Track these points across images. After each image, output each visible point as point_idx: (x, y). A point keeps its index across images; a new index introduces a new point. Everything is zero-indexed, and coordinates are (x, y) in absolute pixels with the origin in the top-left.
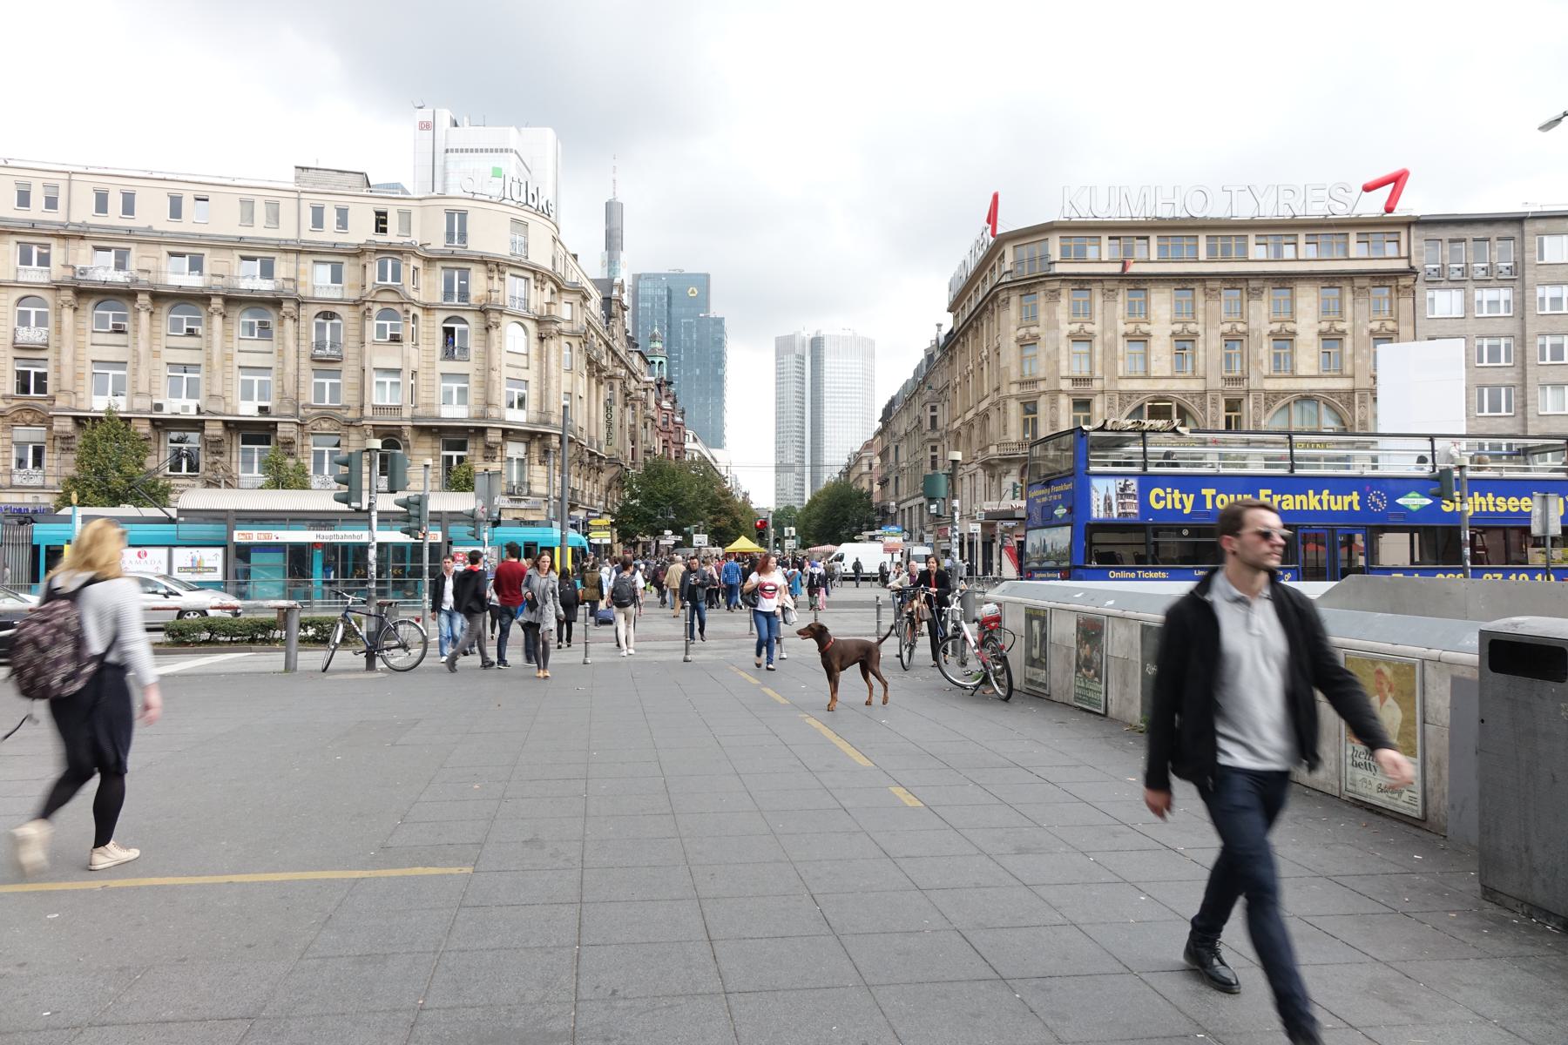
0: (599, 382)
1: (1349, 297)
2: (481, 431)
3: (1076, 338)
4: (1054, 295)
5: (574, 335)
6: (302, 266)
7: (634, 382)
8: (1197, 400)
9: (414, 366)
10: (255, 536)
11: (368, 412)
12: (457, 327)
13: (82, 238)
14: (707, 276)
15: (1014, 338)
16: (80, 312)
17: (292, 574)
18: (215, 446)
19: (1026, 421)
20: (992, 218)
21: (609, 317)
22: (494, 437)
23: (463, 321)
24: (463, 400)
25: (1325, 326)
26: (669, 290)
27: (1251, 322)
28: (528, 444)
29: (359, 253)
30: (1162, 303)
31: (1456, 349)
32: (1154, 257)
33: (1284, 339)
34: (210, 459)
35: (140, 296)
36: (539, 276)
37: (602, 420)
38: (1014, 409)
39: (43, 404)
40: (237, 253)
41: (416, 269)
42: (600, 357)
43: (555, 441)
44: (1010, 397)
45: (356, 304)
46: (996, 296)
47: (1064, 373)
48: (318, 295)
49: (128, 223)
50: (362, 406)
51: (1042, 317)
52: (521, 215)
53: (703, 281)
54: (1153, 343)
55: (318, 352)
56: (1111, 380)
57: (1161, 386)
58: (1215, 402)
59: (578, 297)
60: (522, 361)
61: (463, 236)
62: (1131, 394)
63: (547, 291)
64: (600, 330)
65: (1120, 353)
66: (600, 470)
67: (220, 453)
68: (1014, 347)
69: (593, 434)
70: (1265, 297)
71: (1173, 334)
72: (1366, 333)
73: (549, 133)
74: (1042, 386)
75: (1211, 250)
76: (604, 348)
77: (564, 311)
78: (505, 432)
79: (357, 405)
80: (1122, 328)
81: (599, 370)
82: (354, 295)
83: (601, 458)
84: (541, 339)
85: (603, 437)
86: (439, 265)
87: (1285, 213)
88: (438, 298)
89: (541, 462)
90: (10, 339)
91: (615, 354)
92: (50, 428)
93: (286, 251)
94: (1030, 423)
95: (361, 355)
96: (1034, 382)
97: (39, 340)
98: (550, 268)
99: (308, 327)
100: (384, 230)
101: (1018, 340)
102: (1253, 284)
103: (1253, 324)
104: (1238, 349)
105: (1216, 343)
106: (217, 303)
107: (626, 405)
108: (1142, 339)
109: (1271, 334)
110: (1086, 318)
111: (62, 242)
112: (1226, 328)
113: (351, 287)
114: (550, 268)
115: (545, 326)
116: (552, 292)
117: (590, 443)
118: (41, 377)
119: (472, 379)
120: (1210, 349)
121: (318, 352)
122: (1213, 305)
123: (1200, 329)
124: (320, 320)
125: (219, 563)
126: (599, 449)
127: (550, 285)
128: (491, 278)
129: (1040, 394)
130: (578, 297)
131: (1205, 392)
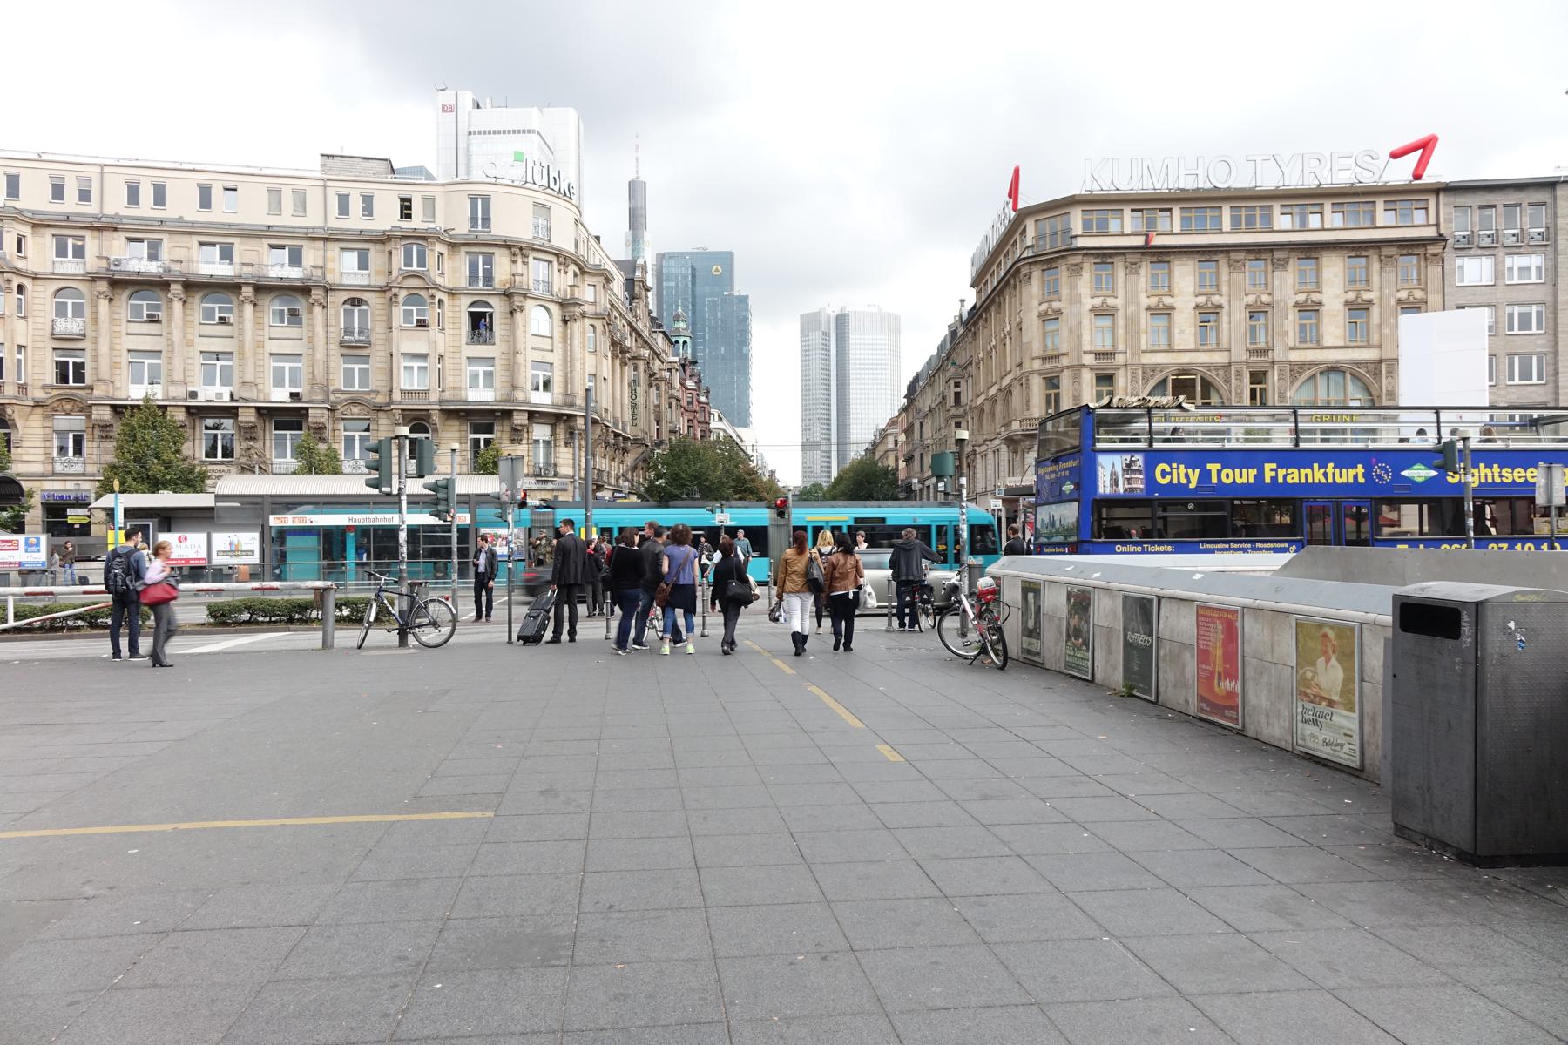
0: (624, 364)
1: (1376, 266)
2: (508, 414)
3: (1098, 312)
4: (1076, 269)
5: (597, 317)
6: (329, 253)
7: (658, 362)
9: (441, 350)
10: (291, 520)
13: (116, 229)
14: (731, 254)
15: (1035, 313)
18: (249, 432)
19: (1049, 396)
20: (1014, 193)
21: (633, 297)
22: (521, 419)
23: (360, 302)
25: (1351, 296)
26: (693, 269)
28: (553, 426)
29: (384, 239)
32: (1177, 229)
33: (1310, 310)
34: (244, 445)
36: (562, 258)
38: (1037, 384)
40: (266, 242)
41: (441, 254)
42: (624, 338)
44: (1033, 372)
45: (383, 290)
46: (1018, 271)
47: (1087, 348)
49: (159, 214)
50: (391, 391)
52: (543, 198)
53: (727, 259)
55: (347, 338)
56: (1134, 354)
57: (1185, 359)
58: (1239, 374)
59: (601, 279)
60: (546, 344)
61: (486, 221)
62: (1155, 368)
63: (570, 274)
64: (624, 311)
65: (1143, 327)
66: (625, 451)
67: (253, 439)
68: (1036, 322)
70: (1290, 267)
71: (1197, 306)
72: (1393, 302)
73: (571, 114)
74: (1065, 361)
75: (1236, 221)
76: (627, 329)
77: (587, 293)
78: (531, 414)
79: (386, 389)
80: (1145, 301)
81: (623, 352)
82: (380, 281)
84: (565, 322)
85: (628, 418)
86: (463, 250)
87: (1311, 183)
88: (463, 283)
89: (566, 444)
91: (639, 335)
93: (314, 239)
96: (1056, 357)
97: (76, 331)
98: (573, 250)
99: (337, 314)
100: (409, 216)
101: (1040, 315)
102: (1278, 254)
104: (1262, 321)
105: (1240, 315)
106: (247, 291)
107: (651, 386)
108: (1166, 312)
111: (96, 233)
112: (1251, 299)
113: (378, 273)
114: (573, 250)
115: (568, 309)
116: (576, 275)
117: (615, 424)
118: (79, 367)
119: (497, 362)
120: (1234, 321)
121: (347, 338)
123: (1223, 301)
125: (256, 547)
126: (624, 429)
127: (572, 268)
128: (514, 262)
129: (1063, 368)
130: (601, 279)
131: (1230, 364)
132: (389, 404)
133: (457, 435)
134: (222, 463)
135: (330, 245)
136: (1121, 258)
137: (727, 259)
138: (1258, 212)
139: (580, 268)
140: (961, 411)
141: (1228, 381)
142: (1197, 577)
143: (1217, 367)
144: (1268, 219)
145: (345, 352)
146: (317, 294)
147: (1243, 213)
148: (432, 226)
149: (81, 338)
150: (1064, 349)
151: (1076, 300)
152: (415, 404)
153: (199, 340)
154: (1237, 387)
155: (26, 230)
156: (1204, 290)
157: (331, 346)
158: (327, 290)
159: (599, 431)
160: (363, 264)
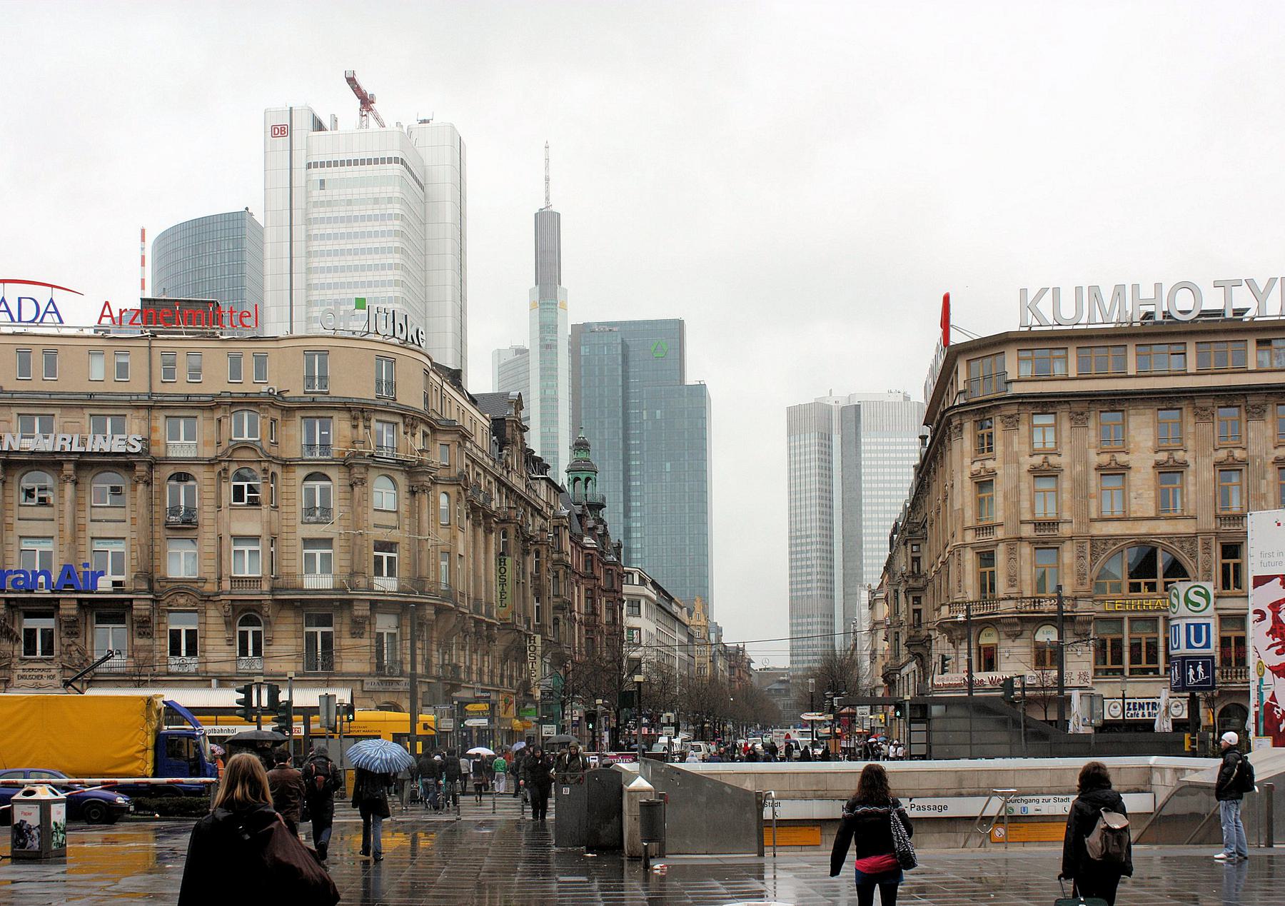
0: (488, 531)
2: (349, 603)
4: (1012, 422)
7: (539, 521)
8: (1187, 545)
11: (226, 585)
14: (680, 324)
15: (967, 474)
16: (80, 486)
18: (72, 627)
19: (1225, 568)
21: (502, 443)
22: (361, 610)
24: (326, 569)
26: (625, 347)
27: (1252, 447)
28: (400, 616)
30: (1142, 431)
34: (66, 641)
36: (411, 419)
38: (969, 558)
43: (430, 612)
44: (964, 546)
45: (211, 463)
46: (949, 422)
47: (1026, 516)
50: (220, 579)
51: (999, 447)
53: (673, 332)
55: (173, 519)
57: (1143, 528)
58: (1207, 547)
59: (455, 437)
60: (391, 520)
62: (1107, 539)
63: (419, 435)
65: (1093, 490)
66: (491, 639)
67: (76, 634)
68: (969, 486)
70: (1269, 417)
71: (1157, 465)
74: (1000, 533)
77: (437, 456)
78: (373, 604)
79: (214, 577)
80: (1095, 460)
81: (486, 516)
82: (209, 453)
83: (490, 626)
84: (413, 493)
86: (299, 414)
91: (510, 490)
94: (986, 585)
95: (217, 521)
96: (990, 528)
99: (162, 491)
101: (973, 476)
102: (1253, 400)
103: (1254, 449)
105: (1208, 474)
106: (69, 469)
107: (526, 552)
108: (1119, 471)
113: (205, 444)
114: (420, 406)
116: (425, 435)
117: (477, 609)
119: (335, 543)
120: (1199, 483)
121: (173, 519)
123: (1188, 457)
124: (174, 483)
128: (355, 427)
132: (218, 594)
133: (292, 628)
134: (41, 660)
135: (155, 413)
137: (673, 332)
139: (431, 427)
140: (921, 583)
141: (1193, 555)
145: (168, 532)
146: (141, 470)
148: (264, 389)
150: (999, 517)
152: (245, 594)
153: (17, 524)
154: (1206, 562)
155: (277, 414)
158: (153, 464)
159: (453, 620)
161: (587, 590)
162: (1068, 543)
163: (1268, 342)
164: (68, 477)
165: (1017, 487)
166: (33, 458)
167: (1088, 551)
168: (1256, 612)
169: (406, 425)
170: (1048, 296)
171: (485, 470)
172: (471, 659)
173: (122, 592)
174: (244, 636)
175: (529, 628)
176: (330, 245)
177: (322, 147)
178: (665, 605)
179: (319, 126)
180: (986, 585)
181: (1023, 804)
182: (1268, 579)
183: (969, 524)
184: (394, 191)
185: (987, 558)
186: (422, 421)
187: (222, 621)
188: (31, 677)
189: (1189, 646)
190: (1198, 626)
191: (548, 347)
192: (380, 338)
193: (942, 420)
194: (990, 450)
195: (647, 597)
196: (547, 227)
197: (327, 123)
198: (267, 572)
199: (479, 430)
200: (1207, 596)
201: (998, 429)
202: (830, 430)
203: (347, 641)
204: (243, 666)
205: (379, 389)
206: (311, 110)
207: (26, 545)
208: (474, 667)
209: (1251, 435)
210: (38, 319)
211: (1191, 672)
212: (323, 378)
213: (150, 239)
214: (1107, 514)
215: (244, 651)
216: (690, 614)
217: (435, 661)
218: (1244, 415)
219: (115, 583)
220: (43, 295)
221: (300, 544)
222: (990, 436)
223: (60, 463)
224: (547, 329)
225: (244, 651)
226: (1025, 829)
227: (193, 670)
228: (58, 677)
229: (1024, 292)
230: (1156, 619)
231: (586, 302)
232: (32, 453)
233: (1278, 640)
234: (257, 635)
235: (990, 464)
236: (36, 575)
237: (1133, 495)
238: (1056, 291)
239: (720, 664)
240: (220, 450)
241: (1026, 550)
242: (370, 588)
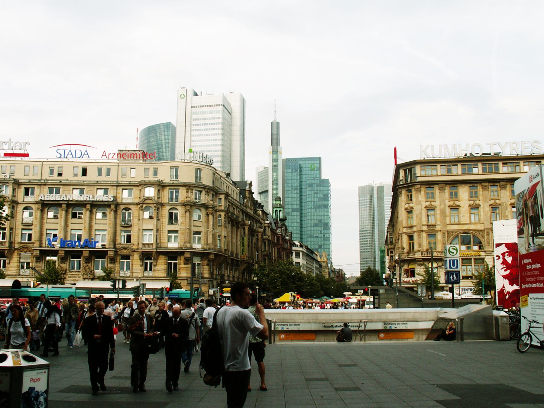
0: (238, 228)
4: (419, 190)
6: (118, 191)
8: (481, 233)
12: (174, 211)
13: (45, 185)
14: (319, 159)
15: (403, 209)
17: (93, 395)
19: (410, 243)
23: (129, 209)
31: (495, 223)
32: (460, 173)
34: (85, 265)
35: (63, 205)
37: (239, 243)
39: (30, 245)
40: (96, 187)
44: (404, 233)
48: (124, 201)
54: (461, 209)
56: (443, 225)
57: (465, 227)
62: (453, 231)
63: (210, 195)
66: (237, 265)
69: (235, 250)
71: (470, 205)
74: (415, 229)
75: (484, 169)
79: (137, 243)
80: (448, 203)
82: (137, 201)
83: (237, 261)
85: (239, 251)
86: (168, 188)
87: (514, 154)
90: (21, 222)
92: (32, 254)
93: (113, 186)
94: (411, 246)
96: (412, 227)
97: (30, 222)
98: (212, 185)
101: (406, 209)
102: (502, 183)
103: (503, 200)
104: (497, 210)
105: (488, 209)
108: (455, 208)
109: (511, 204)
110: (432, 200)
111: (39, 186)
112: (492, 202)
113: (136, 198)
114: (212, 185)
116: (213, 195)
119: (179, 232)
122: (486, 192)
123: (481, 203)
124: (124, 211)
126: (237, 257)
128: (187, 192)
131: (484, 230)
134: (76, 272)
135: (118, 188)
136: (438, 186)
138: (493, 166)
139: (215, 192)
141: (483, 237)
142: (287, 297)
143: (479, 231)
144: (497, 169)
146: (113, 207)
147: (487, 166)
148: (156, 179)
149: (31, 225)
151: (419, 203)
156: (472, 199)
157: (118, 227)
160: (130, 194)
161: (278, 249)
162: (439, 233)
163: (506, 163)
164: (112, 209)
165: (421, 213)
166: (77, 203)
167: (446, 235)
168: (497, 256)
169: (206, 192)
170: (430, 148)
171: (237, 207)
172: (230, 273)
173: (105, 248)
174: (146, 263)
175: (253, 262)
176: (198, 133)
177: (196, 101)
178: (310, 254)
179: (196, 94)
180: (411, 246)
181: (282, 326)
182: (501, 244)
183: (404, 226)
184: (220, 115)
185: (411, 238)
186: (211, 190)
187: (139, 258)
188: (72, 277)
189: (450, 267)
190: (453, 261)
191: (275, 167)
192: (196, 162)
193: (396, 189)
194: (411, 200)
195: (302, 252)
196: (275, 128)
197: (198, 93)
198: (155, 242)
199: (235, 194)
200: (456, 250)
201: (414, 193)
202: (373, 194)
203: (183, 266)
204: (146, 274)
205: (196, 179)
206: (241, 96)
207: (73, 232)
208: (231, 276)
209: (502, 195)
210: (81, 156)
211: (451, 277)
212: (200, 177)
213: (139, 131)
214: (453, 222)
215: (146, 269)
216: (321, 257)
217: (215, 273)
218: (499, 188)
219: (102, 245)
220: (83, 149)
221: (167, 232)
222: (411, 195)
223: (86, 204)
224: (275, 160)
225: (146, 269)
226: (391, 335)
227: (128, 275)
228: (82, 277)
229: (421, 146)
230: (471, 259)
231: (288, 152)
232: (77, 201)
233: (505, 266)
234: (151, 263)
235: (411, 205)
236: (75, 242)
237: (461, 216)
238: (433, 146)
239: (332, 275)
240: (140, 200)
241: (424, 235)
242: (191, 247)
